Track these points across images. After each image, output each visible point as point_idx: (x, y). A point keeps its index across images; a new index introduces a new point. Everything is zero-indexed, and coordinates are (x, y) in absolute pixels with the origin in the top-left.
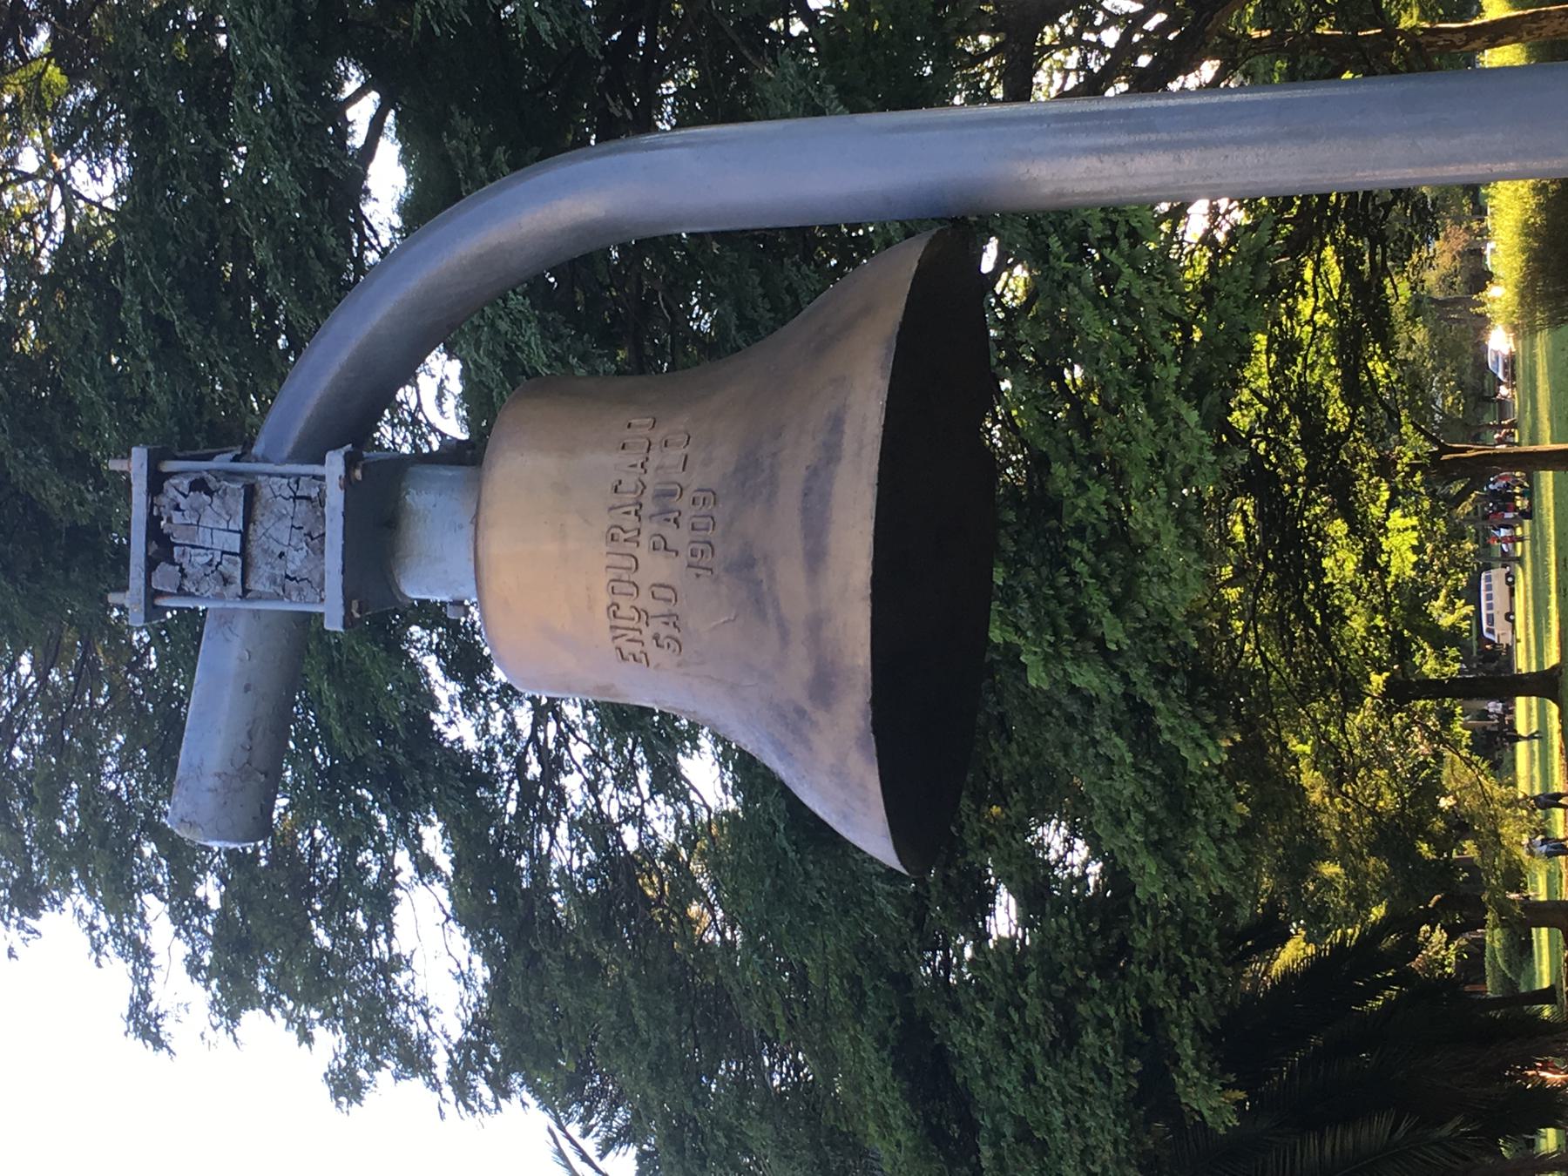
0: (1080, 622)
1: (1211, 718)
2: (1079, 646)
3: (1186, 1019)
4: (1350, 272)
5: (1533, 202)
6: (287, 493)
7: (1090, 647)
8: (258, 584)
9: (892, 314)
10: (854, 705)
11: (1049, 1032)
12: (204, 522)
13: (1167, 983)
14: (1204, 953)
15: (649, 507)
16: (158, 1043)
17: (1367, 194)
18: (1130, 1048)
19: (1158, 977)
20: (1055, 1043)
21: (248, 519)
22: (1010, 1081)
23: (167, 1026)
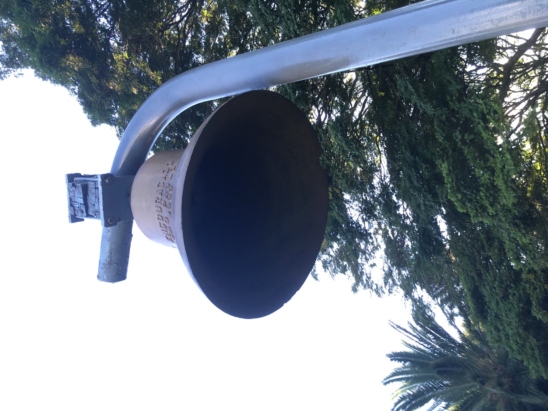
0: (484, 209)
1: (524, 232)
2: (483, 214)
3: (535, 296)
6: (94, 187)
7: (486, 214)
11: (501, 295)
13: (530, 288)
14: (540, 282)
16: (317, 279)
18: (520, 300)
19: (528, 285)
20: (503, 298)
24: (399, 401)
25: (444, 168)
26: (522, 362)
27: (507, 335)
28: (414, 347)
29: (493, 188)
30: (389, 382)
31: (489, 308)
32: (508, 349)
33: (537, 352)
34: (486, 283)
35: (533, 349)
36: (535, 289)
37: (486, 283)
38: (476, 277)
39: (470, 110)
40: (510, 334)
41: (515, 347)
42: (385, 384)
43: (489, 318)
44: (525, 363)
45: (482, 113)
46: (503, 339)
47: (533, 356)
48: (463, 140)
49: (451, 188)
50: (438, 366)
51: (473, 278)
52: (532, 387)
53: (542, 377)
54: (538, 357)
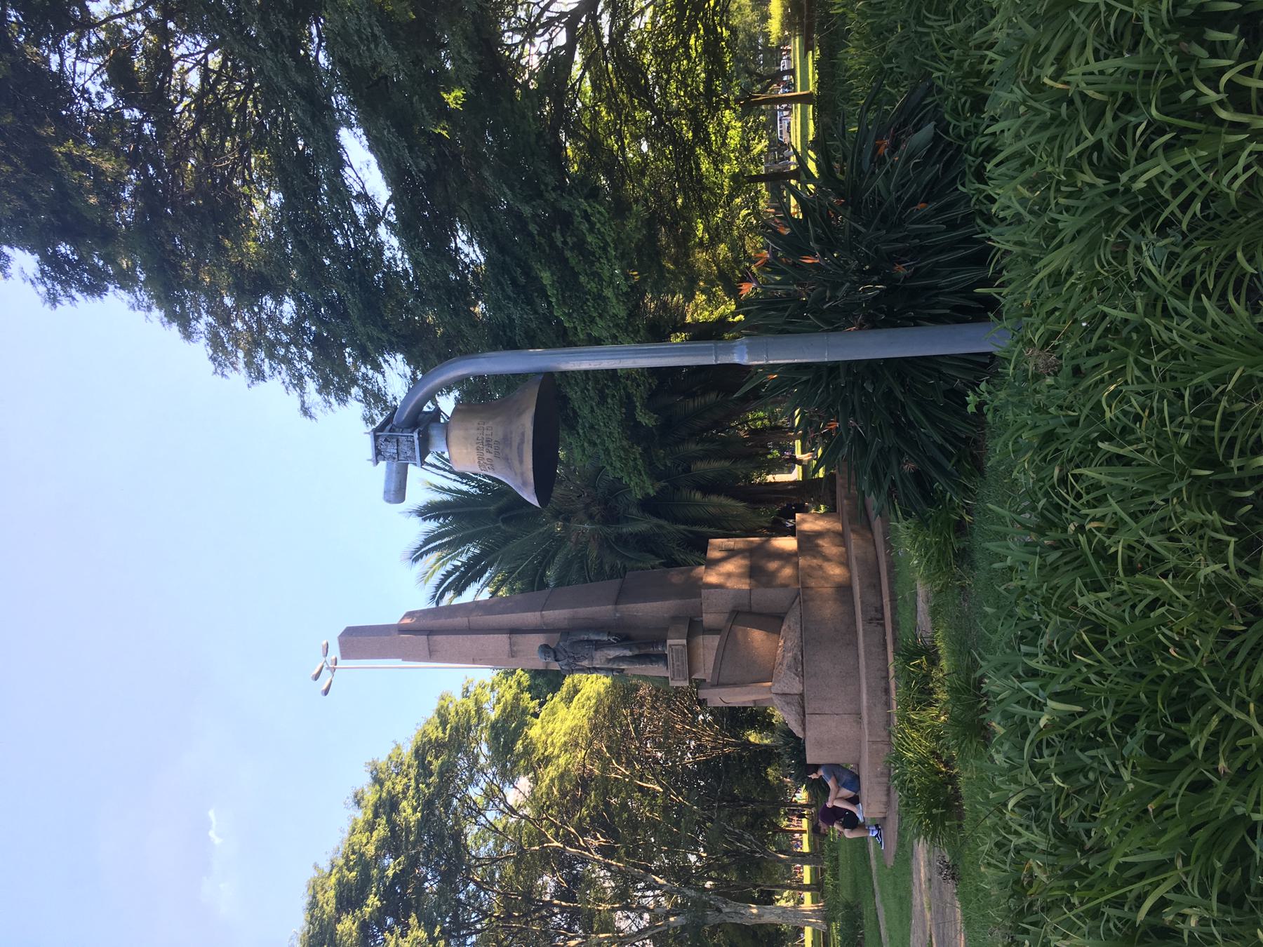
9: (533, 410)
10: (532, 488)
19: (629, 382)
22: (586, 411)
23: (313, 410)
24: (443, 581)
25: (546, 277)
26: (620, 479)
28: (450, 490)
29: (600, 297)
30: (421, 556)
33: (640, 462)
36: (638, 385)
41: (618, 465)
42: (416, 560)
45: (586, 211)
46: (602, 456)
47: (635, 468)
48: (565, 243)
50: (500, 511)
52: (634, 511)
53: (648, 494)
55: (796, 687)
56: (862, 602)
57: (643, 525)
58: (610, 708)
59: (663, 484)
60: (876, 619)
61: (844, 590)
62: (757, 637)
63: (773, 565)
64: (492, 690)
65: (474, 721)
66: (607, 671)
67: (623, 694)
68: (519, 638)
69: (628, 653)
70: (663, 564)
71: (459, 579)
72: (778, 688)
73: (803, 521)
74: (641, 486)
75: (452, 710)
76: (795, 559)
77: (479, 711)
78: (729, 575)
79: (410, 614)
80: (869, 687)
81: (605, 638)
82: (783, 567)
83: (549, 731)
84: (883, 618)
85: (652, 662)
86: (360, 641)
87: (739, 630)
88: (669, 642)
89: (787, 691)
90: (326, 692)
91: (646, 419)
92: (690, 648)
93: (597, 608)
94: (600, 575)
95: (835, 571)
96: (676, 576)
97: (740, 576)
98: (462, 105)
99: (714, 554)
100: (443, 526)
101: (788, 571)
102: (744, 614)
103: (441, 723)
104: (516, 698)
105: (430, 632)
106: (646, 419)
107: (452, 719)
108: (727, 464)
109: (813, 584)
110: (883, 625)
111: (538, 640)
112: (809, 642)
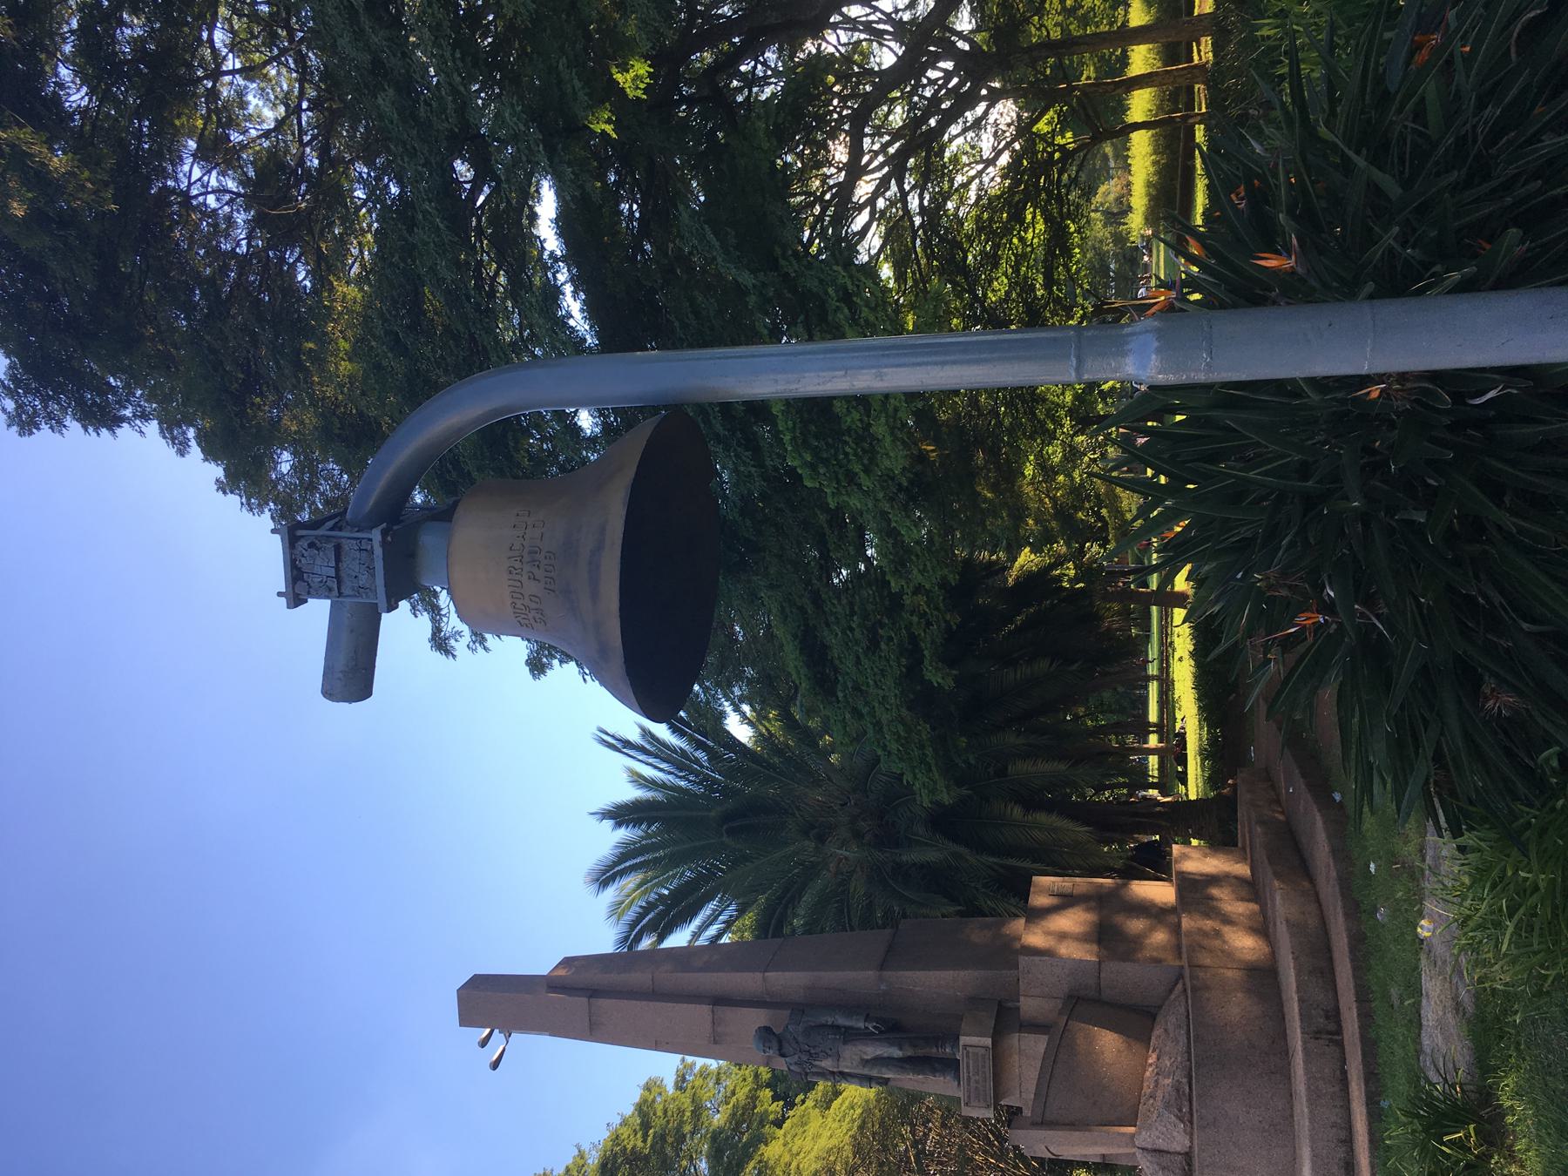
0: (851, 478)
4: (1011, 473)
5: (1152, 169)
8: (346, 591)
9: (631, 472)
12: (318, 562)
14: (937, 609)
15: (527, 558)
17: (887, 396)
21: (338, 559)
24: (640, 917)
27: (878, 725)
30: (612, 879)
31: (836, 670)
32: (879, 752)
33: (929, 751)
34: (832, 619)
35: (922, 747)
37: (832, 619)
38: (810, 609)
39: (821, 281)
40: (884, 722)
41: (894, 746)
43: (840, 695)
44: (908, 777)
45: (845, 288)
49: (794, 439)
50: (727, 817)
51: (802, 609)
54: (932, 762)
55: (1178, 1140)
56: (1301, 1000)
57: (930, 854)
58: (882, 1124)
59: (965, 792)
60: (1326, 1031)
61: (1263, 977)
62: (1108, 1043)
63: (1136, 925)
64: (718, 1082)
65: (687, 1128)
66: (866, 1080)
67: (904, 1107)
68: (728, 1013)
69: (896, 1053)
70: (961, 914)
71: (661, 915)
72: (1146, 1138)
73: (1185, 856)
74: (931, 790)
75: (659, 1108)
76: (1172, 919)
77: (698, 1111)
78: (1063, 936)
79: (567, 962)
80: (1315, 1156)
81: (861, 1025)
82: (1152, 929)
83: (795, 1150)
84: (1339, 1031)
85: (934, 1071)
86: (494, 1002)
87: (1076, 1025)
88: (964, 1040)
89: (1161, 1144)
90: (495, 1065)
91: (937, 676)
92: (998, 1057)
93: (851, 975)
94: (867, 923)
95: (1245, 943)
96: (977, 933)
97: (1083, 938)
98: (645, 91)
99: (1039, 900)
100: (648, 836)
101: (1160, 937)
102: (1088, 1002)
103: (642, 1124)
104: (753, 1098)
105: (593, 992)
106: (937, 676)
107: (658, 1123)
108: (1062, 767)
109: (1208, 961)
110: (1340, 1045)
111: (757, 1018)
112: (1207, 1060)
